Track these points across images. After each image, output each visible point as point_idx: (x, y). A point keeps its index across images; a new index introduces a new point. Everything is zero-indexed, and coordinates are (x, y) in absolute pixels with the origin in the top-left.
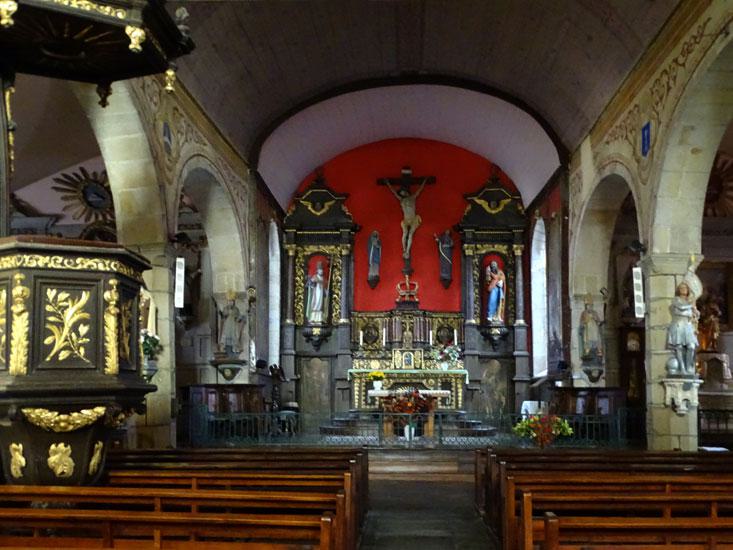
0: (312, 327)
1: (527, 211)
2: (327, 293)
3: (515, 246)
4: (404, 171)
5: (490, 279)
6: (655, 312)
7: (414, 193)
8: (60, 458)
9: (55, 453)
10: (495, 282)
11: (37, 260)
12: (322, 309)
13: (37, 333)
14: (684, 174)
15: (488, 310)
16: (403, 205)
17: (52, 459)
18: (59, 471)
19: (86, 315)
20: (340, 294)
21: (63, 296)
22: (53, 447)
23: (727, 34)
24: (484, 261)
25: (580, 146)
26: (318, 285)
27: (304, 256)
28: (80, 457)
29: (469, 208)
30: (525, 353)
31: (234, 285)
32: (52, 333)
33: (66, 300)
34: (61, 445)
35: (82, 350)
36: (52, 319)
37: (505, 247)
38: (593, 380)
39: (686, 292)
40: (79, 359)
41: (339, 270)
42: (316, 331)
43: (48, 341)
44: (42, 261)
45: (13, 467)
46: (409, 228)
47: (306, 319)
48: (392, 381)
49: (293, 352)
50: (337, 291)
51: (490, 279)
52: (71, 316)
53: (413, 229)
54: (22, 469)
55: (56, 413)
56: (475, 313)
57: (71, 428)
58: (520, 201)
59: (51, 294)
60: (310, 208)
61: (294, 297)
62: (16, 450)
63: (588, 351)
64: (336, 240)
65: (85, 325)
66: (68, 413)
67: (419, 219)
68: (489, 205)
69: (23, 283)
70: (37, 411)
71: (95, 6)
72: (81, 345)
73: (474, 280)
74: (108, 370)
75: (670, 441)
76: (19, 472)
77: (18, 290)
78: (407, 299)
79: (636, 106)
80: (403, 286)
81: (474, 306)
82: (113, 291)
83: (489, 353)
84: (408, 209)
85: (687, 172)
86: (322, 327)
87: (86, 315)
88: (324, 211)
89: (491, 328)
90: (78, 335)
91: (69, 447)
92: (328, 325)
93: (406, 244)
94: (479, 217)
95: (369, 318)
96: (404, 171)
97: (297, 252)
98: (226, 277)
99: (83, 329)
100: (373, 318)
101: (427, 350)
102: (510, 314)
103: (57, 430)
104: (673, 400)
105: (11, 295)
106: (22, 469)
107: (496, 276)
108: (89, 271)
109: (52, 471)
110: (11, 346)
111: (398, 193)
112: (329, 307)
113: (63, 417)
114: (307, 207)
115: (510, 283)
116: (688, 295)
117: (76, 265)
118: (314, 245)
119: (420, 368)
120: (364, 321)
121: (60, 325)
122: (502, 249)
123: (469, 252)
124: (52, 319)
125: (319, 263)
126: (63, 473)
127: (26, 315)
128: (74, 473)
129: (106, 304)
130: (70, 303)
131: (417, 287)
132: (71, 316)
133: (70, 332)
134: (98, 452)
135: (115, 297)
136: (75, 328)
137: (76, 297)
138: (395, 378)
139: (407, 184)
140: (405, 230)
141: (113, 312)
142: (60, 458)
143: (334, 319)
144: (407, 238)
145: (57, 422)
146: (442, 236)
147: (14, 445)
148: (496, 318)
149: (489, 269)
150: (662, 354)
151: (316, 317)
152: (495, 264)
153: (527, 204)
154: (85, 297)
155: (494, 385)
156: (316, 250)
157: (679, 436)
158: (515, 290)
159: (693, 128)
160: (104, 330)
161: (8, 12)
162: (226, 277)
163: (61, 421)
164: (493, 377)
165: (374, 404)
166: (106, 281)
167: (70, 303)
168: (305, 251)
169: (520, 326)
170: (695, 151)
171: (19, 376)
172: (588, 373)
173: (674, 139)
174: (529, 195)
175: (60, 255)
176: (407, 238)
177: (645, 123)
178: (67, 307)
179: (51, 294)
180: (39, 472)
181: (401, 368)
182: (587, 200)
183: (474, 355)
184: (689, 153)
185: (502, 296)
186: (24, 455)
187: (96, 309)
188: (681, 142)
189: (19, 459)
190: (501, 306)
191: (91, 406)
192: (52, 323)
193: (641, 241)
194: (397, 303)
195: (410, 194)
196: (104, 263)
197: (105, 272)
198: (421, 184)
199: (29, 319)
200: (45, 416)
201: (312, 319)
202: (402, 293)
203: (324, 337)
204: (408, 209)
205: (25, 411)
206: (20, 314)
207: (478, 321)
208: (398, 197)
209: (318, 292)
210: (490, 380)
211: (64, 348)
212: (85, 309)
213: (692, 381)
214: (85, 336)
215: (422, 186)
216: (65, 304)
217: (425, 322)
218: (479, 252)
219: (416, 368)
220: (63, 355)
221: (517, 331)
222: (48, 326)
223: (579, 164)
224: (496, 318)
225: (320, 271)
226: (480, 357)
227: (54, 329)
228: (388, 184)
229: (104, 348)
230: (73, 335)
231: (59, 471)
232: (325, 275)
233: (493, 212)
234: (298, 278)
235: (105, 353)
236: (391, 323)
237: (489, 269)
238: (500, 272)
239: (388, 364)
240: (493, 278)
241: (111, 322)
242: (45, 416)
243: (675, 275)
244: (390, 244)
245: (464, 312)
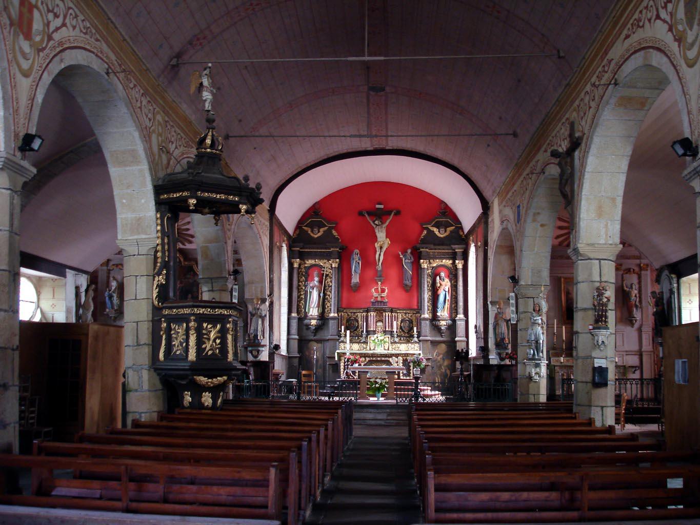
0: (310, 319)
1: (466, 236)
2: (322, 295)
3: (457, 261)
4: (378, 206)
5: (439, 285)
6: (522, 320)
7: (385, 223)
8: (207, 399)
9: (205, 396)
10: (442, 288)
11: (200, 310)
12: (318, 306)
13: (200, 342)
14: (538, 238)
15: (437, 308)
16: (377, 231)
17: (203, 399)
18: (206, 404)
19: (219, 335)
20: (332, 295)
21: (210, 326)
22: (204, 393)
23: (544, 173)
24: (435, 275)
25: (493, 201)
26: (315, 289)
27: (305, 267)
28: (215, 399)
29: (425, 232)
30: (464, 339)
31: (259, 293)
32: (205, 343)
33: (211, 328)
34: (207, 393)
35: (218, 351)
36: (205, 336)
37: (451, 262)
38: (502, 359)
39: (538, 310)
40: (216, 355)
41: (331, 278)
42: (314, 322)
43: (204, 346)
44: (202, 311)
45: (185, 402)
46: (381, 248)
47: (306, 313)
48: (368, 359)
49: (297, 337)
50: (328, 293)
51: (439, 285)
52: (212, 335)
53: (384, 249)
54: (190, 403)
55: (206, 378)
56: (428, 310)
57: (212, 385)
58: (461, 228)
59: (205, 325)
60: (309, 232)
61: (299, 297)
62: (187, 394)
63: (498, 340)
64: (328, 256)
65: (219, 339)
66: (212, 378)
67: (388, 241)
68: (439, 231)
69: (194, 321)
70: (200, 377)
71: (226, 196)
72: (217, 348)
73: (428, 286)
74: (229, 360)
75: (528, 397)
76: (188, 405)
77: (192, 324)
78: (379, 299)
79: (515, 191)
80: (377, 290)
81: (427, 304)
82: (231, 324)
83: (438, 339)
84: (381, 235)
85: (539, 237)
86: (318, 320)
87: (219, 335)
88: (319, 234)
89: (439, 320)
90: (216, 343)
91: (210, 394)
92: (323, 317)
93: (379, 260)
94: (432, 240)
95: (351, 313)
96: (378, 206)
97: (300, 265)
98: (254, 288)
99: (218, 341)
100: (354, 313)
101: (392, 336)
102: (454, 310)
103: (207, 386)
104: (529, 373)
105: (189, 326)
106: (190, 403)
107: (443, 283)
108: (221, 314)
109: (203, 404)
110: (189, 348)
111: (374, 222)
112: (323, 304)
113: (210, 380)
114: (307, 231)
115: (454, 287)
116: (539, 310)
117: (215, 312)
118: (311, 259)
119: (388, 350)
120: (348, 315)
121: (209, 339)
122: (448, 262)
123: (425, 266)
124: (205, 336)
125: (316, 273)
126: (208, 405)
127: (195, 335)
128: (212, 406)
129: (228, 329)
130: (212, 329)
131: (387, 291)
132: (212, 335)
133: (213, 343)
134: (221, 397)
135: (232, 327)
136: (214, 340)
137: (214, 327)
138: (369, 357)
139: (380, 215)
140: (378, 249)
141: (231, 333)
142: (207, 399)
143: (326, 315)
144: (380, 255)
145: (207, 383)
146: (404, 252)
147: (186, 392)
148: (443, 313)
149: (438, 278)
150: (526, 346)
151: (314, 312)
152: (443, 274)
153: (466, 231)
154: (219, 326)
155: (441, 362)
156: (314, 263)
157: (534, 395)
158: (456, 293)
159: (539, 213)
160: (227, 342)
161: (193, 204)
162: (254, 288)
163: (209, 382)
164: (441, 356)
165: (409, 376)
166: (228, 320)
167: (212, 329)
168: (305, 263)
169: (460, 320)
170: (542, 225)
171: (192, 362)
172: (499, 354)
173: (530, 219)
174: (467, 224)
175: (209, 308)
176: (380, 255)
177: (518, 204)
178: (211, 331)
179: (205, 325)
180: (197, 404)
181: (374, 350)
182: (497, 238)
183: (427, 341)
184: (539, 226)
185: (448, 298)
186: (190, 397)
187: (223, 334)
188: (534, 220)
189: (188, 398)
190: (447, 305)
191: (221, 376)
192: (206, 338)
193: (517, 278)
194: (371, 302)
195: (383, 223)
196: (227, 311)
197: (228, 315)
198: (390, 215)
199: (197, 336)
200: (203, 380)
201: (310, 313)
202: (375, 295)
203: (319, 328)
204: (381, 235)
205: (195, 377)
206: (192, 334)
207: (431, 315)
208: (373, 225)
209: (315, 294)
210: (439, 358)
211: (209, 350)
212: (219, 332)
213: (540, 362)
214: (219, 344)
215: (391, 217)
216: (211, 330)
217: (392, 317)
218: (432, 265)
219: (385, 350)
220: (210, 353)
221: (458, 322)
222: (204, 340)
223: (493, 214)
224: (443, 313)
225: (316, 279)
226: (432, 342)
227: (206, 341)
228: (367, 216)
229: (227, 349)
230: (214, 343)
231: (206, 404)
232: (320, 282)
233: (442, 236)
234: (301, 283)
235: (227, 352)
236: (367, 317)
237: (438, 278)
238: (447, 280)
239: (365, 346)
240: (441, 284)
241: (230, 337)
242: (203, 380)
243: (533, 298)
244: (368, 262)
245: (419, 310)
